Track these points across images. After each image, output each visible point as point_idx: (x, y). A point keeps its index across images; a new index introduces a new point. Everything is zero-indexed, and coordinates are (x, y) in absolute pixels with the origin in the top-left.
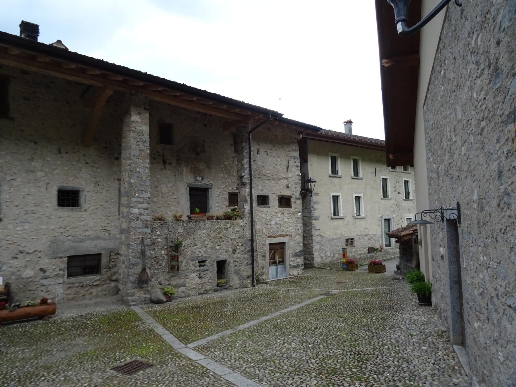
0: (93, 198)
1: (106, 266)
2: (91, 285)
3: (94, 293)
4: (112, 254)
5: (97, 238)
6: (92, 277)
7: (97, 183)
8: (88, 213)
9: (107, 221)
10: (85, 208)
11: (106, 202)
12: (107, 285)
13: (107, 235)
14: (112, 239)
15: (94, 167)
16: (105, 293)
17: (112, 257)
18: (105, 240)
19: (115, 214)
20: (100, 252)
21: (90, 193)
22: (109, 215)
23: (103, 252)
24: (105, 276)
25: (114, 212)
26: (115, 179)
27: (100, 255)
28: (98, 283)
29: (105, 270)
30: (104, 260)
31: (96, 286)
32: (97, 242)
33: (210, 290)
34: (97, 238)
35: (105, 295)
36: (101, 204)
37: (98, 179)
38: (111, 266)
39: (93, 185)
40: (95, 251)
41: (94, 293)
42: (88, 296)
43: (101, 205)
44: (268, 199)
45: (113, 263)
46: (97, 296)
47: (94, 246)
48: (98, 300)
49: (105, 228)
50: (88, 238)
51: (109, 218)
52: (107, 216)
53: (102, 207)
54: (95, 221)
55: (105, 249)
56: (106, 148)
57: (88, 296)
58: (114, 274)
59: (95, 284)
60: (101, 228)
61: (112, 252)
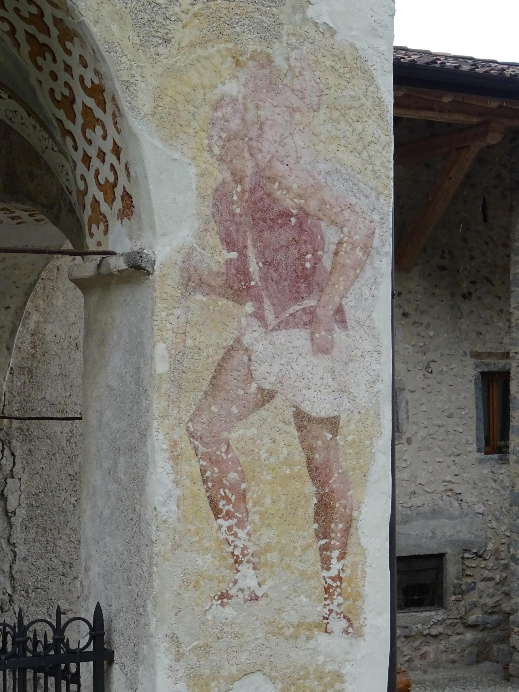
0: (424, 408)
1: (455, 586)
2: (425, 636)
3: (431, 657)
4: (467, 555)
5: (436, 513)
6: (428, 614)
7: (428, 367)
8: (415, 445)
9: (453, 467)
10: (408, 435)
11: (450, 416)
12: (457, 637)
13: (456, 504)
14: (467, 515)
15: (421, 324)
16: (452, 656)
17: (467, 562)
18: (451, 518)
19: (470, 448)
20: (442, 551)
21: (417, 395)
22: (457, 452)
23: (449, 551)
24: (455, 614)
25: (467, 442)
26: (465, 354)
27: (440, 557)
28: (440, 629)
29: (454, 598)
30: (452, 570)
31: (435, 637)
32: (434, 523)
33: (10, 531)
34: (436, 513)
35: (454, 662)
36: (440, 422)
37: (430, 356)
38: (464, 587)
39: (420, 374)
40: (430, 547)
41: (431, 657)
42: (417, 663)
43: (439, 426)
44: (85, 24)
45: (469, 580)
46: (436, 666)
47: (430, 535)
48: (441, 674)
49: (450, 486)
50: (418, 514)
51: (457, 459)
52: (453, 454)
53: (442, 430)
54: (430, 469)
55: (452, 543)
56: (443, 268)
57: (417, 663)
58: (471, 609)
59: (434, 632)
60: (442, 488)
61: (466, 551)
